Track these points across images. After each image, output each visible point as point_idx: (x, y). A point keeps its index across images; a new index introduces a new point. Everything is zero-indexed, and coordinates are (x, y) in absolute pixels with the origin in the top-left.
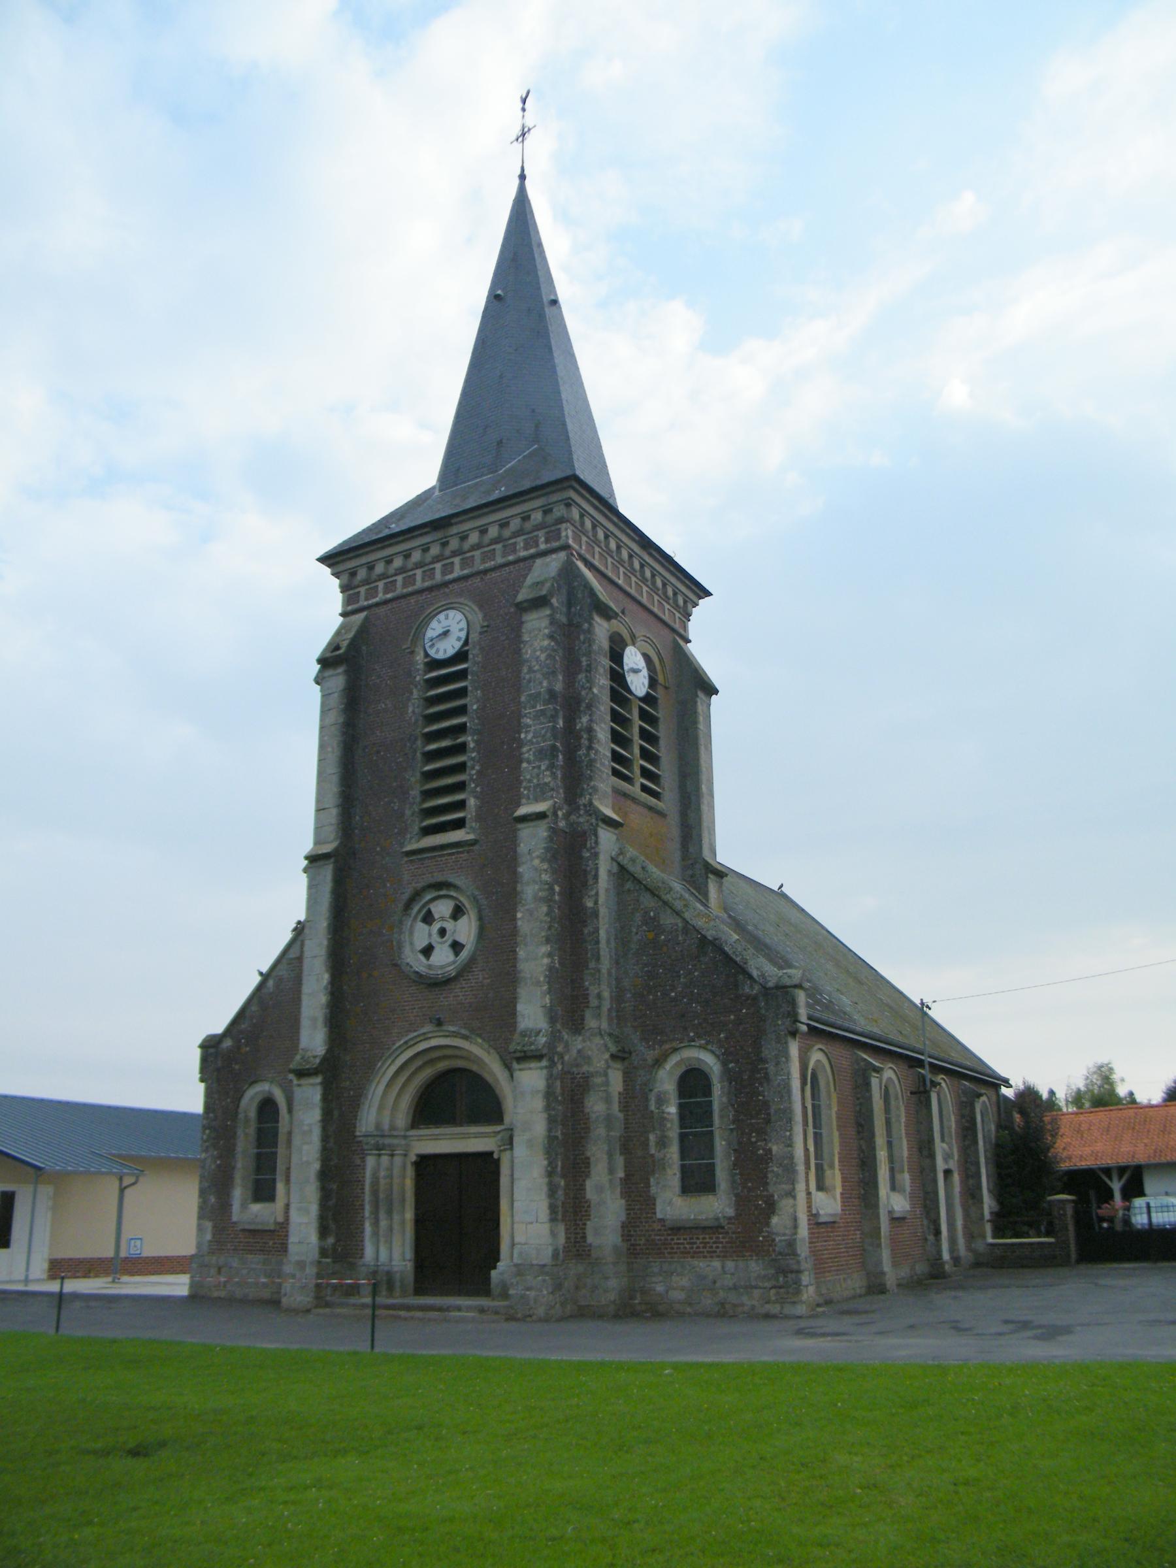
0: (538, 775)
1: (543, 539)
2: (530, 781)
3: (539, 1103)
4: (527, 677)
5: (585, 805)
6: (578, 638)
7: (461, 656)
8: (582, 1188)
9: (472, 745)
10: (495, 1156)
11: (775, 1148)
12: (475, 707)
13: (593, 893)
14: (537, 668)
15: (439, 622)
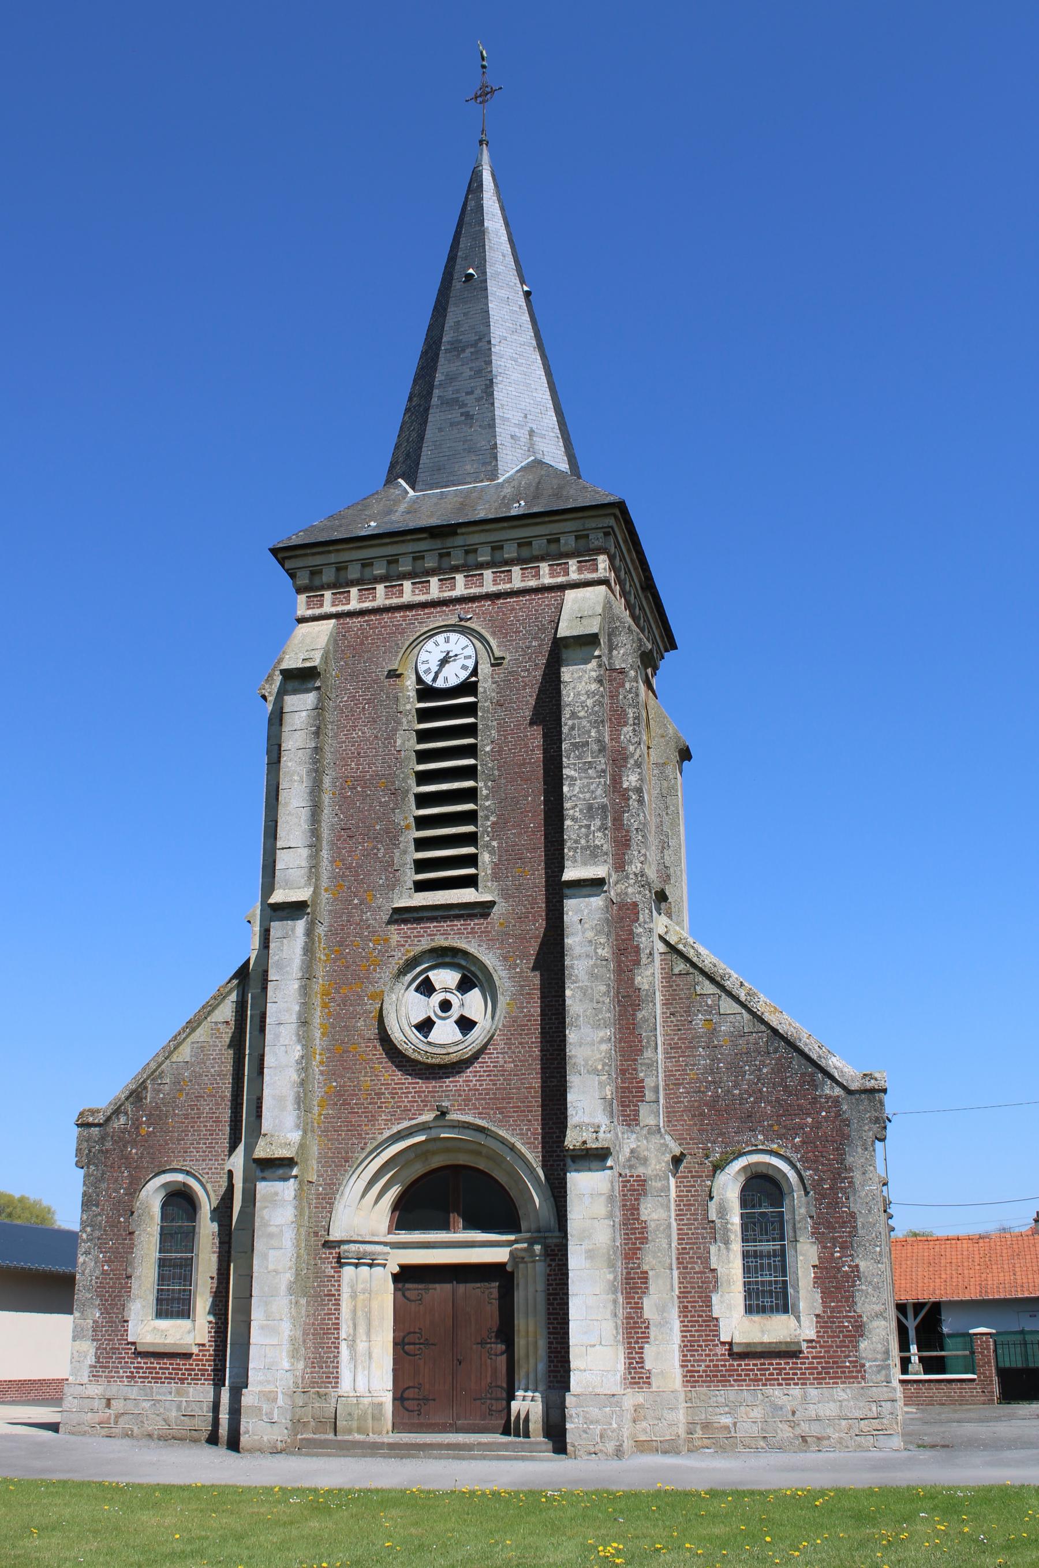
0: (587, 836)
1: (575, 568)
2: (576, 842)
3: (601, 1208)
4: (570, 722)
5: (636, 875)
6: (623, 686)
7: (468, 687)
8: (638, 1308)
9: (485, 792)
10: (509, 1269)
11: (863, 1265)
12: (488, 749)
13: (648, 973)
14: (582, 714)
15: (437, 645)
